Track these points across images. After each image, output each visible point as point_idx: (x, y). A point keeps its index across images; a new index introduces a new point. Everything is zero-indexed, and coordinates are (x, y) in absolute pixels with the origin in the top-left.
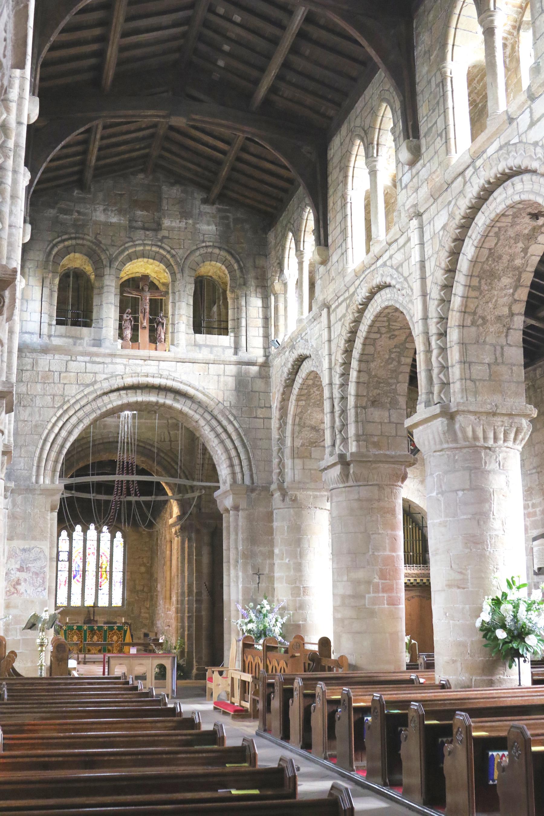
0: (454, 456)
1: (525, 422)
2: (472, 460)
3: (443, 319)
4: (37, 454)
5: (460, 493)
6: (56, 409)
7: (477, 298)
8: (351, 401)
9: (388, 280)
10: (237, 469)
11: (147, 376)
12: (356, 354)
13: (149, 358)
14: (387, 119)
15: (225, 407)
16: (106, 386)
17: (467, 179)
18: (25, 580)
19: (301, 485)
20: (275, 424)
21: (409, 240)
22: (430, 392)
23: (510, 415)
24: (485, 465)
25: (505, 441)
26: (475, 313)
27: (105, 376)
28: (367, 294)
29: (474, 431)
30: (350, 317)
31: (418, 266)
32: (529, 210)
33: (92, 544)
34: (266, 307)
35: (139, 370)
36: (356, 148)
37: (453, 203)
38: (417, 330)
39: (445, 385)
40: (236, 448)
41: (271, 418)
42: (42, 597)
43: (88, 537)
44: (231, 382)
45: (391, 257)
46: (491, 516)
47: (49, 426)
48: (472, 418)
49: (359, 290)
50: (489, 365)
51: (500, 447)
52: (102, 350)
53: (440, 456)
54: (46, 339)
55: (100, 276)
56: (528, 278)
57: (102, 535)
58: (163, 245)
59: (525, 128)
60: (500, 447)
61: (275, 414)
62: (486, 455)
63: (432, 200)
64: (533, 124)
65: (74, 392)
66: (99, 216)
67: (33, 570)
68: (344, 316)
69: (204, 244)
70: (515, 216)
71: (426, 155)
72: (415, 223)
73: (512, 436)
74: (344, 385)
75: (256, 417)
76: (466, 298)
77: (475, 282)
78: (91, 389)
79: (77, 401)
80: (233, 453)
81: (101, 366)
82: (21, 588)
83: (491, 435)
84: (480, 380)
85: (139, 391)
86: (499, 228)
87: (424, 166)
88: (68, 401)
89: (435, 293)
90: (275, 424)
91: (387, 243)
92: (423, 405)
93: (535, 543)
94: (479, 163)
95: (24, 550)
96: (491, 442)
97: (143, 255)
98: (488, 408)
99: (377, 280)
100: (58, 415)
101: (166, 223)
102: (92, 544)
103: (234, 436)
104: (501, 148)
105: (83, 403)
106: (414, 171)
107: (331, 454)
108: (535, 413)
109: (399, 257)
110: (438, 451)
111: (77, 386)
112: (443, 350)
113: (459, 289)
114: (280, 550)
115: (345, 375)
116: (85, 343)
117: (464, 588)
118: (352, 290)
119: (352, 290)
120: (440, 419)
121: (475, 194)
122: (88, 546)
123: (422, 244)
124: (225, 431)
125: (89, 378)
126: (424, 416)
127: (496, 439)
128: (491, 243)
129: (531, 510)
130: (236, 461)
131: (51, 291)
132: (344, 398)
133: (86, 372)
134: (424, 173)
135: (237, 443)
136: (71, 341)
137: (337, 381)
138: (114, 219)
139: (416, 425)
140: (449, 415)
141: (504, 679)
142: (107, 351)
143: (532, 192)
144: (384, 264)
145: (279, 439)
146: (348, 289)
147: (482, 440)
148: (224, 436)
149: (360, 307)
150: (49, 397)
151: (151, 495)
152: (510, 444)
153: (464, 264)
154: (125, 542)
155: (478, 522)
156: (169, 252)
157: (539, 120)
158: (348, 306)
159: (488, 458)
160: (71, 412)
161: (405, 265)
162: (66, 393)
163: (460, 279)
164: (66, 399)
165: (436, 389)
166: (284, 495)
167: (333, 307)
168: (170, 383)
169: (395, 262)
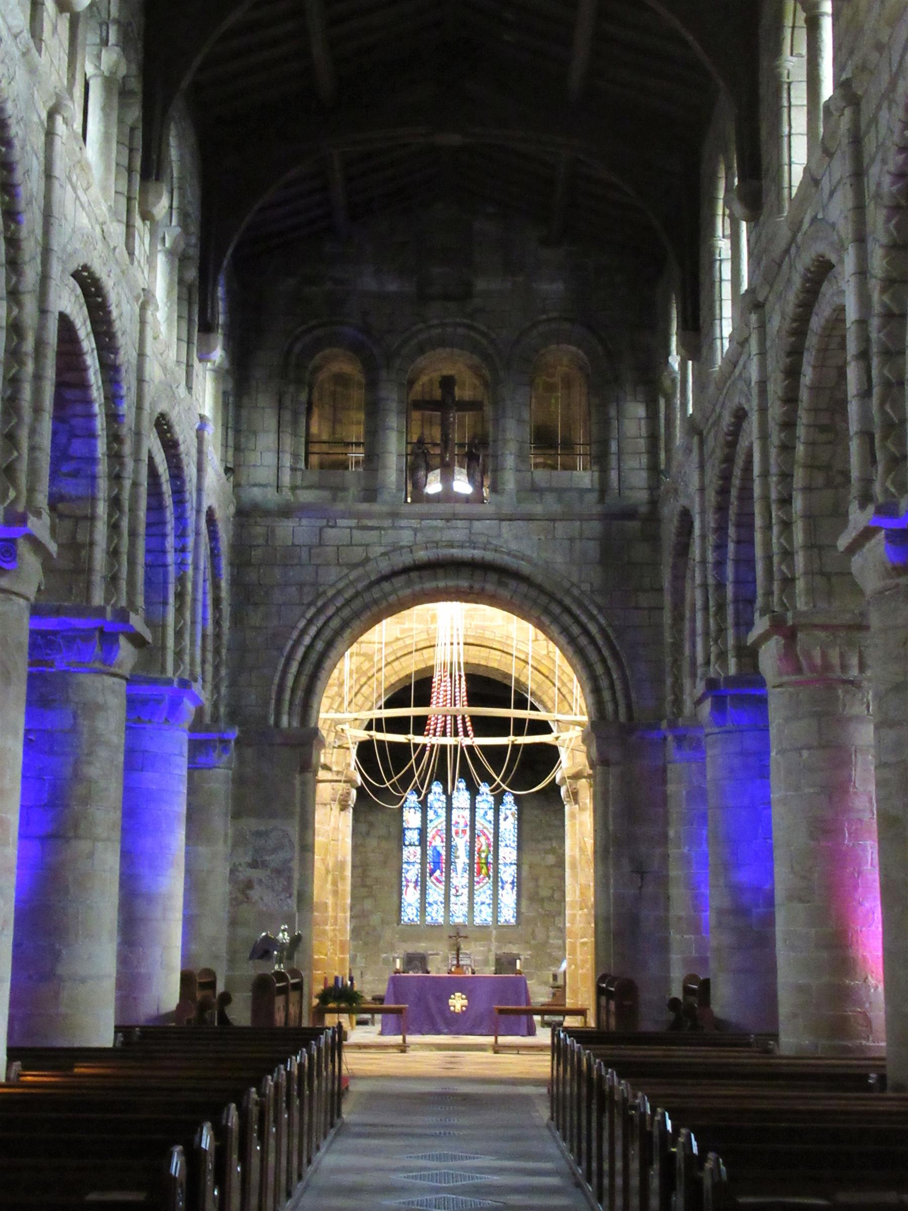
4: (276, 680)
5: (805, 753)
6: (304, 607)
7: (830, 443)
10: (607, 695)
11: (452, 547)
15: (583, 592)
16: (384, 566)
18: (261, 881)
24: (844, 709)
26: (828, 468)
27: (382, 550)
28: (733, 420)
29: (824, 655)
33: (461, 816)
34: (652, 416)
35: (438, 536)
39: (788, 582)
41: (662, 609)
42: (286, 908)
43: (455, 803)
44: (593, 549)
46: (851, 789)
47: (295, 634)
48: (822, 635)
52: (376, 507)
53: (780, 693)
54: (287, 495)
55: (372, 384)
57: (479, 798)
58: (475, 324)
62: (846, 692)
65: (333, 578)
66: (369, 283)
67: (273, 865)
69: (544, 317)
74: (720, 564)
75: (637, 608)
76: (811, 444)
78: (360, 571)
79: (339, 592)
80: (599, 670)
81: (375, 533)
82: (255, 894)
83: (854, 661)
84: (837, 574)
85: (440, 572)
88: (324, 592)
91: (738, 343)
95: (258, 834)
97: (442, 343)
98: (847, 618)
100: (309, 615)
101: (481, 285)
102: (461, 816)
105: (348, 594)
110: (778, 686)
111: (338, 569)
112: (787, 525)
114: (676, 832)
116: (351, 496)
117: (809, 902)
118: (718, 410)
122: (454, 818)
124: (586, 632)
125: (358, 554)
127: (862, 667)
130: (604, 683)
131: (295, 414)
132: (720, 586)
133: (351, 545)
135: (606, 653)
136: (326, 494)
138: (392, 287)
142: (385, 509)
145: (673, 644)
146: (714, 410)
147: (838, 669)
148: (583, 641)
149: (729, 438)
150: (294, 589)
151: (507, 735)
155: (830, 798)
159: (848, 697)
160: (330, 611)
162: (321, 580)
164: (321, 589)
168: (489, 556)
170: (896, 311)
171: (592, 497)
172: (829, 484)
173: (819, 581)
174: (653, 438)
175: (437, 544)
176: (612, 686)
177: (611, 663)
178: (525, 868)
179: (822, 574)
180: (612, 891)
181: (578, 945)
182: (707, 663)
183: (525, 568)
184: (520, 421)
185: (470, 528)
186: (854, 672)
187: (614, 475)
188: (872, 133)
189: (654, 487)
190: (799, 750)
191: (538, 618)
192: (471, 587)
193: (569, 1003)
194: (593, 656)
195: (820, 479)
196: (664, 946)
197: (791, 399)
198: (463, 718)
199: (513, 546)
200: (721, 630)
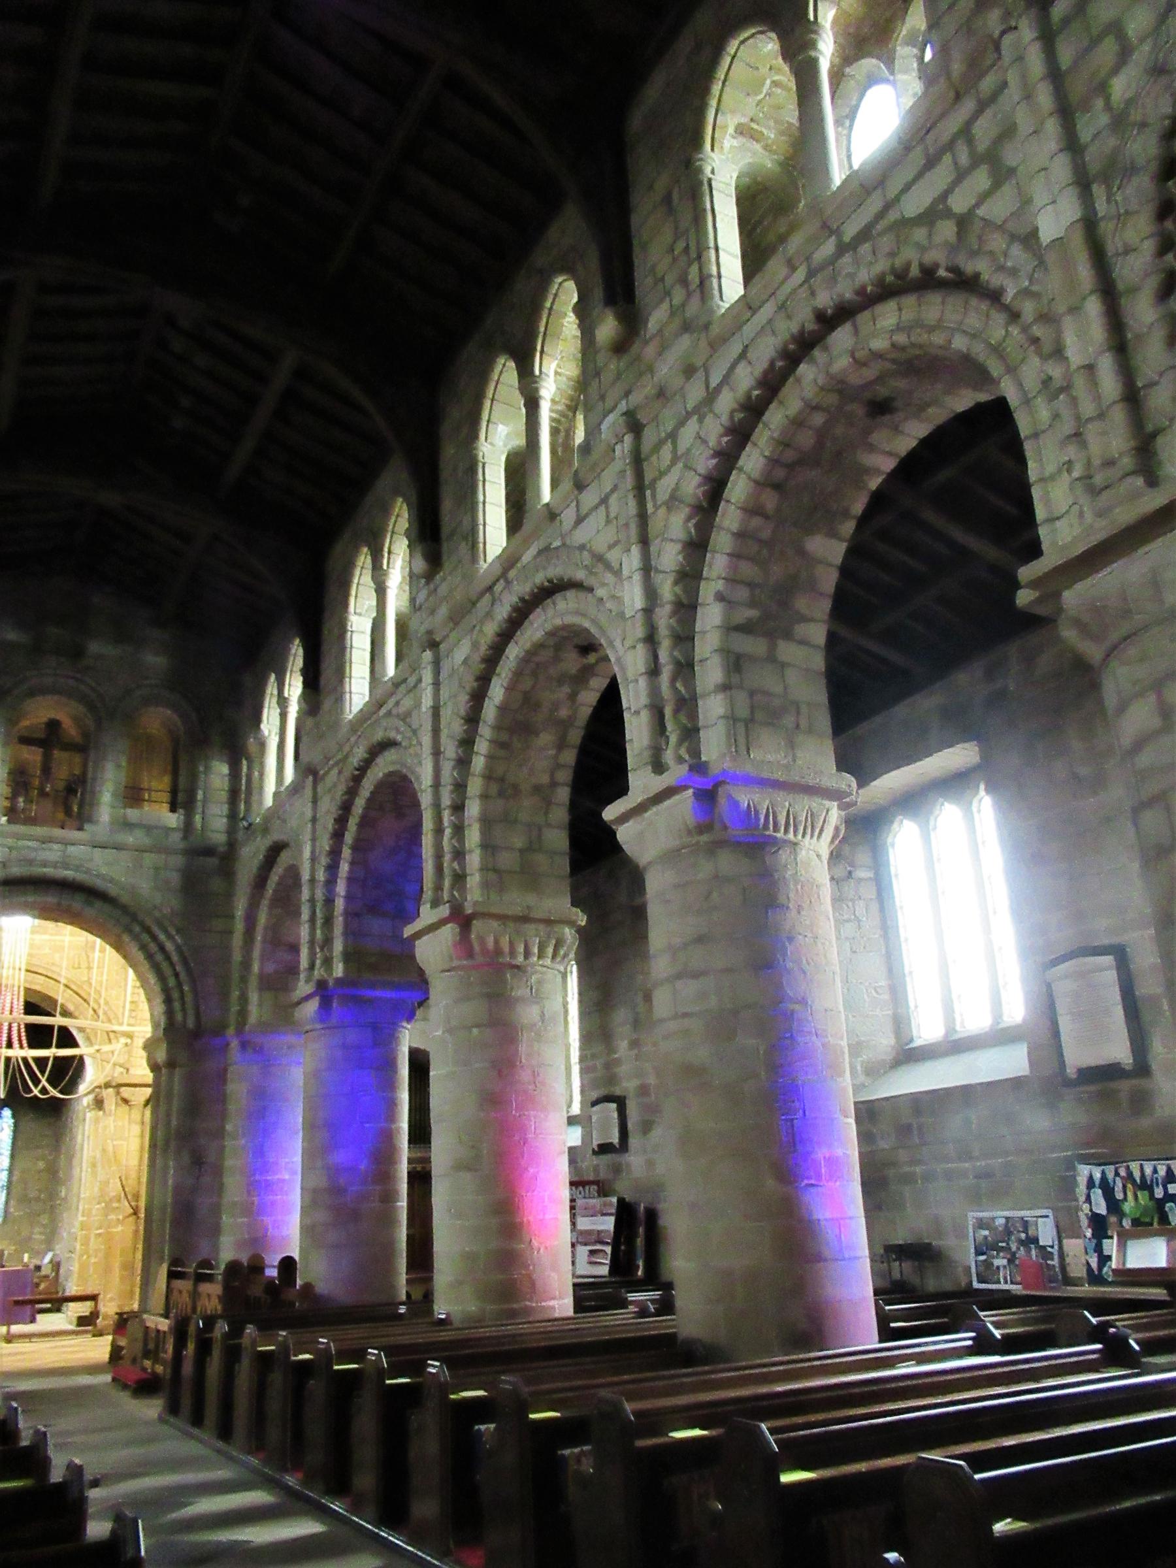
0: (469, 978)
1: (569, 933)
2: (496, 987)
3: (460, 787)
5: (475, 1031)
8: (340, 904)
9: (392, 735)
10: (177, 1005)
12: (349, 838)
13: (51, 840)
14: (401, 517)
17: (497, 595)
19: (266, 1028)
20: (237, 940)
21: (420, 680)
22: (438, 888)
23: (548, 922)
25: (539, 957)
26: (502, 780)
28: (366, 756)
29: (496, 942)
30: (341, 788)
31: (430, 713)
32: (576, 641)
34: (235, 775)
36: (362, 558)
37: (478, 628)
38: (426, 800)
39: (460, 878)
40: (177, 975)
44: (175, 878)
45: (397, 703)
48: (495, 924)
49: (356, 750)
50: (521, 851)
51: (533, 965)
56: (576, 736)
59: (570, 527)
60: (533, 965)
61: (239, 926)
63: (451, 625)
64: (580, 520)
68: (335, 785)
70: (558, 648)
71: (447, 565)
72: (428, 655)
73: (550, 950)
74: (331, 882)
76: (490, 757)
77: (504, 737)
80: (172, 982)
83: (521, 949)
86: (537, 664)
87: (444, 579)
89: (450, 750)
90: (237, 940)
92: (428, 906)
93: (594, 1109)
94: (512, 574)
96: (520, 959)
98: (517, 910)
99: (379, 735)
101: (95, 647)
103: (175, 958)
104: (540, 552)
106: (432, 586)
107: (307, 982)
108: (582, 920)
109: (407, 703)
110: (448, 971)
113: (482, 746)
115: (333, 868)
118: (347, 748)
119: (347, 748)
120: (449, 925)
121: (505, 615)
123: (437, 684)
124: (162, 948)
126: (430, 922)
127: (527, 954)
128: (527, 684)
129: (591, 1063)
130: (176, 995)
132: (329, 901)
134: (443, 589)
137: (321, 876)
139: (418, 935)
140: (462, 919)
141: (532, 1308)
143: (578, 613)
144: (389, 713)
145: (241, 963)
148: (159, 957)
151: (49, 1046)
152: (548, 962)
153: (490, 712)
154: (16, 1125)
156: (93, 689)
157: (587, 515)
158: (340, 772)
161: (415, 714)
163: (485, 731)
165: (447, 883)
166: (244, 1045)
167: (322, 772)
168: (80, 877)
169: (402, 709)
170: (685, 601)
171: (176, 837)
172: (501, 794)
173: (492, 876)
174: (234, 793)
175: (31, 862)
176: (182, 997)
177: (183, 976)
178: (17, 1173)
179: (495, 870)
180: (170, 1182)
181: (92, 1236)
182: (312, 967)
183: (113, 891)
184: (119, 766)
185: (64, 851)
186: (520, 959)
187: (198, 818)
188: (654, 458)
189: (231, 830)
190: (469, 1028)
191: (119, 936)
192: (59, 904)
193: (72, 1289)
194: (168, 971)
195: (494, 789)
196: (215, 1231)
197: (473, 719)
198: (19, 1026)
199: (104, 870)
200: (328, 941)
